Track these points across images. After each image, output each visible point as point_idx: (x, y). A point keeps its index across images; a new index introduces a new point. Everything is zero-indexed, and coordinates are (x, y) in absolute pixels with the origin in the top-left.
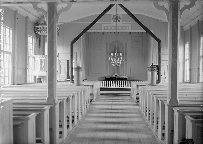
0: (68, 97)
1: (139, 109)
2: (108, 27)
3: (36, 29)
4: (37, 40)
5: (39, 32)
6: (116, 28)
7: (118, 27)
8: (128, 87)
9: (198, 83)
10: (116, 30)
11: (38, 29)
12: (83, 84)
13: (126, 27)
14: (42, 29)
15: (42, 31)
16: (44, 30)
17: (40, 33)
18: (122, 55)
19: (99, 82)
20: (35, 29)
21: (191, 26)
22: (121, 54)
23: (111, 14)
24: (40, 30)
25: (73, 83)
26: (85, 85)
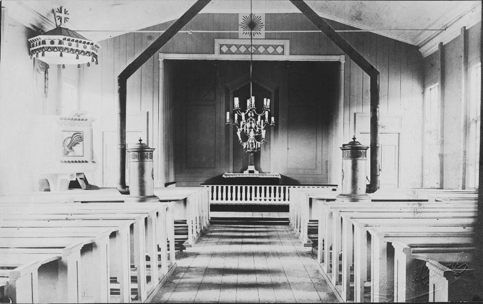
0: (59, 255)
1: (321, 271)
2: (229, 46)
3: (33, 46)
4: (37, 76)
5: (40, 54)
6: (250, 49)
7: (255, 46)
8: (282, 202)
9: (463, 191)
10: (250, 55)
11: (37, 46)
12: (154, 196)
13: (275, 47)
14: (48, 44)
15: (49, 50)
16: (53, 49)
17: (43, 55)
18: (268, 104)
19: (207, 189)
20: (29, 45)
21: (465, 27)
22: (265, 103)
23: (238, 14)
24: (44, 47)
25: (128, 193)
26: (161, 199)
